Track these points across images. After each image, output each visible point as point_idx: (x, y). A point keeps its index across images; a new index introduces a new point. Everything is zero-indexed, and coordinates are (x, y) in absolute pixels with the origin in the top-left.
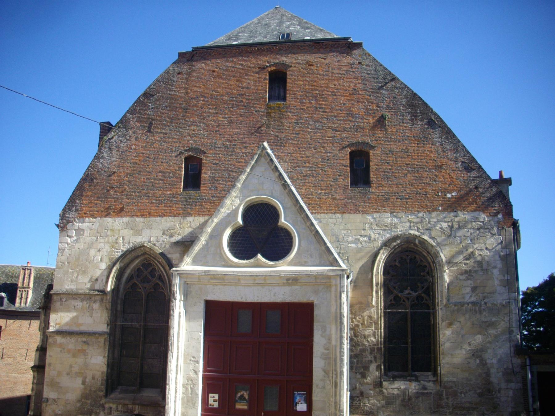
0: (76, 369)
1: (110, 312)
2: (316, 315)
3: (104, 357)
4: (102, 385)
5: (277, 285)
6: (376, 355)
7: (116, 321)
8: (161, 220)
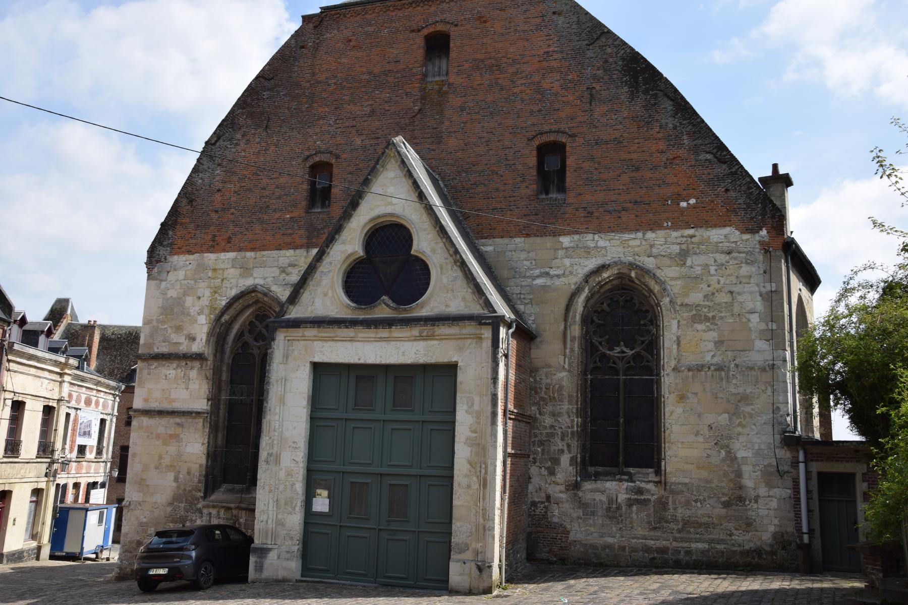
0: (167, 461)
3: (203, 444)
4: (199, 482)
5: (407, 339)
6: (570, 441)
8: (277, 254)
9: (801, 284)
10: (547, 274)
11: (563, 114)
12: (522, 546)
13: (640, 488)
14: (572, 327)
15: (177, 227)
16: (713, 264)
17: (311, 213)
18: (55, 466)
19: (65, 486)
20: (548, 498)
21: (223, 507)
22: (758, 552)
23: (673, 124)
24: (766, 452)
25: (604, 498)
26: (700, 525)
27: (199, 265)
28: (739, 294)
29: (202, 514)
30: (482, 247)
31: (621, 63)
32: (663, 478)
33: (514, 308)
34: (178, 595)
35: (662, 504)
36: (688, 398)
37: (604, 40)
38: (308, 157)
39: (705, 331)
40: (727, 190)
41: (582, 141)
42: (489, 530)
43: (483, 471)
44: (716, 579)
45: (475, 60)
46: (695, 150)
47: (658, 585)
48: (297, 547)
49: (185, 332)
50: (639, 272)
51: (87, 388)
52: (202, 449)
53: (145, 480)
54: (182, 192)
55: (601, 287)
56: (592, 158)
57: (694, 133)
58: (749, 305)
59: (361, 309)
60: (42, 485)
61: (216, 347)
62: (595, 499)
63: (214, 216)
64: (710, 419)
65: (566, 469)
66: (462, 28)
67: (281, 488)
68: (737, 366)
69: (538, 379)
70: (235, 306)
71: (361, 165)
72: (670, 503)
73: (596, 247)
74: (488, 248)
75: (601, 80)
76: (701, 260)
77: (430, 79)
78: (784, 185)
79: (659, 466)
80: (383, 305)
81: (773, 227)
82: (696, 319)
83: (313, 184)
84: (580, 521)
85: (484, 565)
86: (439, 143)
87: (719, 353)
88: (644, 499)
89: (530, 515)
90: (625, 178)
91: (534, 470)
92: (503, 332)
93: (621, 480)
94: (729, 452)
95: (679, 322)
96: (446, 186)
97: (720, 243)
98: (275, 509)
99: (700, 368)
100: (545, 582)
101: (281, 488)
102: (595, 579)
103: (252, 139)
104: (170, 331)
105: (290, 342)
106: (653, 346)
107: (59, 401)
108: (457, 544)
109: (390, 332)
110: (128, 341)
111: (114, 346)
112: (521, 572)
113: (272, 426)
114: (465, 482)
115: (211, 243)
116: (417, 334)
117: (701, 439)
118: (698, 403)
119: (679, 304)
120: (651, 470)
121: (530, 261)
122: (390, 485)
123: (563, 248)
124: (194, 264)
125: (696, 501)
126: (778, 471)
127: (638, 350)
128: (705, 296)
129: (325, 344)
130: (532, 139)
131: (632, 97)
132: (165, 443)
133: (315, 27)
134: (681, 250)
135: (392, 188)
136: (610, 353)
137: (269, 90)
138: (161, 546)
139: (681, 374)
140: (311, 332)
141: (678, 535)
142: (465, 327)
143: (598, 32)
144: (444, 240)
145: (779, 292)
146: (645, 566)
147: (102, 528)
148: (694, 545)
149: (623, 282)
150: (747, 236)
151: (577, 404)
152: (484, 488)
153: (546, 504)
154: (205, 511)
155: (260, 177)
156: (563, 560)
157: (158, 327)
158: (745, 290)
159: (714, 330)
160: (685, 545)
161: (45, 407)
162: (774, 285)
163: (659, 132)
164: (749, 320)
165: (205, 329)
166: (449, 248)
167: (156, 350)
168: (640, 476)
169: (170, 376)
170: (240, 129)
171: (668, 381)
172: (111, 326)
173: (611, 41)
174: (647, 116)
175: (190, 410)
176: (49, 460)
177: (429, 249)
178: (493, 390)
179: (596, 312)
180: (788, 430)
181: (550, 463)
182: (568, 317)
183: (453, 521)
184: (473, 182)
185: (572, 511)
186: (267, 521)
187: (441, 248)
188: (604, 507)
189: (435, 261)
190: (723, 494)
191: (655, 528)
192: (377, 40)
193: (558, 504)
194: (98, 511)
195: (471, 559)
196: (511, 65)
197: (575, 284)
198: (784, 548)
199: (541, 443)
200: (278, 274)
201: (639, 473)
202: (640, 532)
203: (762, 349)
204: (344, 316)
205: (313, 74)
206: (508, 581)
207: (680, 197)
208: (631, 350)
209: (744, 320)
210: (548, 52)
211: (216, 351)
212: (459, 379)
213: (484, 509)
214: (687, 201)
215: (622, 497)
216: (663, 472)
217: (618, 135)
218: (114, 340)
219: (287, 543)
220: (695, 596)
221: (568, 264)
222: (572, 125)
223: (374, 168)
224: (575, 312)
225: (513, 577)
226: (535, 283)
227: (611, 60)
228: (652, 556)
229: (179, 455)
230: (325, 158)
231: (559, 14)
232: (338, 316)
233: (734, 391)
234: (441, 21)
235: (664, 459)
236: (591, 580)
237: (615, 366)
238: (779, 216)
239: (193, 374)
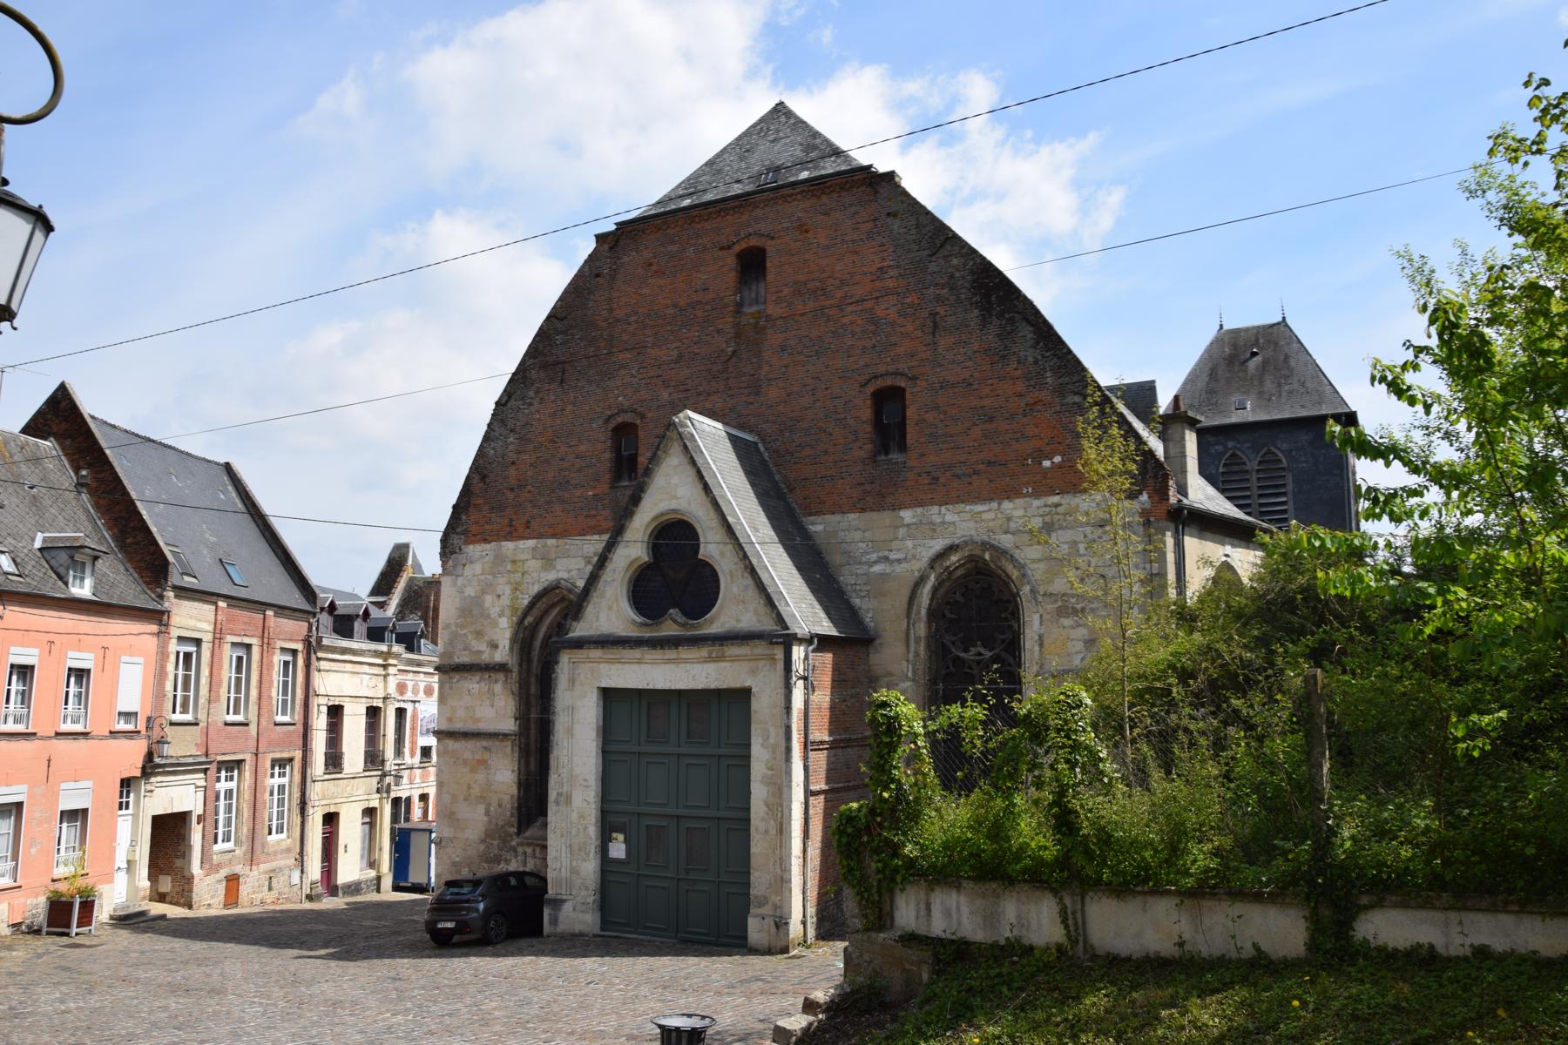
0: (476, 791)
1: (517, 698)
2: (755, 712)
3: (513, 771)
4: (512, 815)
7: (528, 712)
10: (886, 559)
11: (901, 350)
14: (917, 625)
16: (1083, 539)
18: (388, 780)
19: (408, 800)
21: (538, 845)
27: (496, 557)
38: (610, 417)
39: (1073, 628)
41: (924, 384)
45: (796, 282)
48: (592, 898)
51: (425, 673)
56: (936, 408)
57: (1060, 367)
60: (375, 804)
61: (521, 656)
63: (510, 495)
70: (538, 606)
73: (943, 523)
76: (1068, 535)
77: (747, 310)
81: (1155, 490)
82: (1063, 611)
86: (757, 394)
95: (1041, 616)
96: (767, 449)
101: (574, 832)
103: (546, 398)
104: (470, 637)
106: (1014, 646)
107: (385, 699)
108: (757, 897)
109: (678, 653)
123: (904, 525)
124: (491, 554)
129: (611, 666)
130: (866, 384)
131: (984, 323)
132: (473, 770)
133: (611, 248)
134: (1045, 523)
135: (676, 477)
136: (962, 655)
137: (562, 333)
140: (596, 653)
142: (755, 646)
143: (942, 238)
154: (520, 850)
161: (369, 709)
163: (1016, 369)
165: (508, 634)
167: (457, 660)
170: (532, 384)
173: (957, 248)
176: (379, 773)
179: (948, 603)
189: (725, 568)
196: (839, 288)
197: (919, 570)
200: (583, 565)
205: (611, 310)
207: (1042, 454)
208: (991, 651)
210: (881, 269)
211: (521, 660)
214: (1051, 459)
221: (911, 546)
222: (913, 364)
223: (655, 454)
224: (919, 606)
226: (872, 570)
227: (958, 274)
229: (489, 784)
232: (624, 634)
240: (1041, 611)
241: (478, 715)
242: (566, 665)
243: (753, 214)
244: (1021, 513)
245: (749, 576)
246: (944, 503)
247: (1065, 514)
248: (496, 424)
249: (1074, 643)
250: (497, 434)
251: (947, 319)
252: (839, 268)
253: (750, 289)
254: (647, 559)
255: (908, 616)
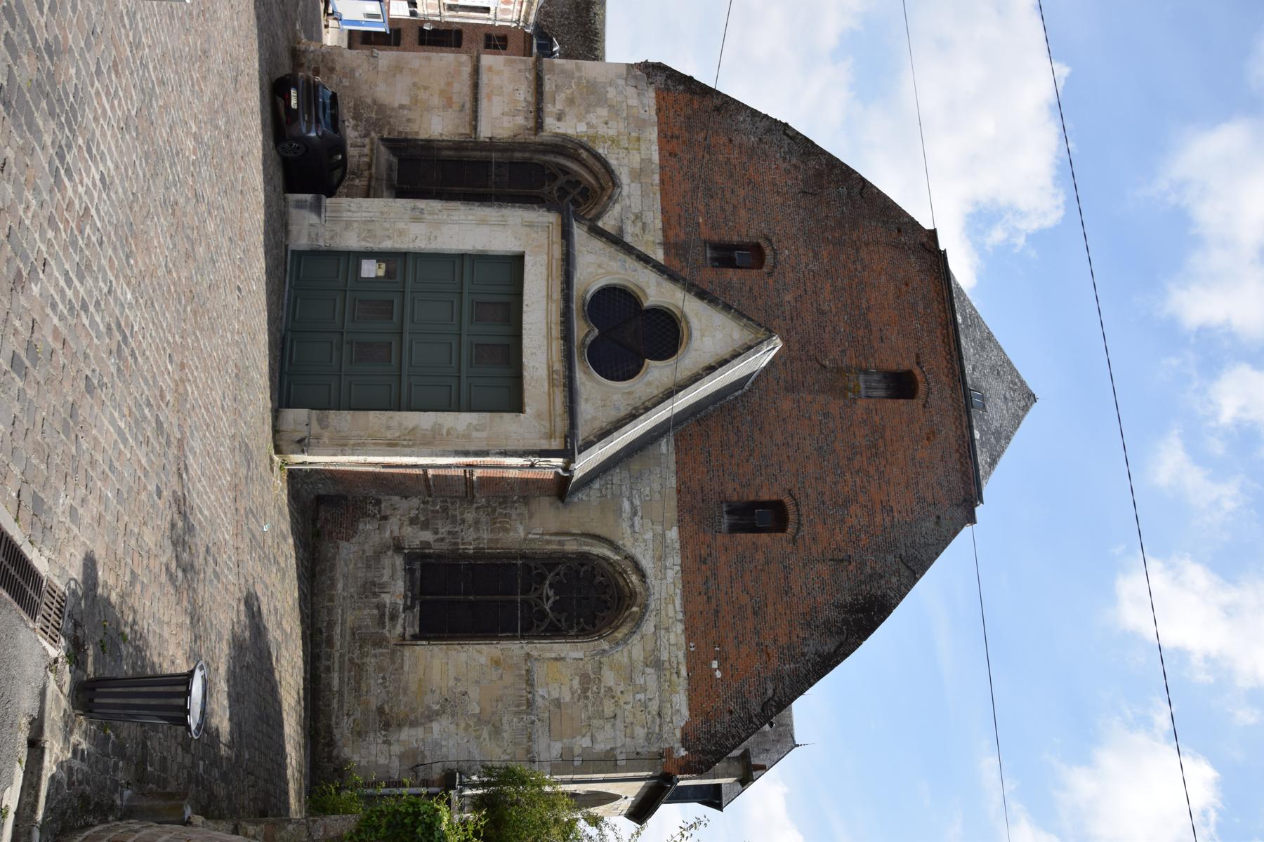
0: (423, 95)
1: (510, 140)
2: (501, 417)
3: (441, 135)
4: (400, 133)
9: (633, 799)
10: (635, 514)
12: (331, 490)
13: (397, 617)
14: (575, 542)
15: (688, 95)
16: (647, 697)
17: (705, 246)
20: (385, 518)
21: (371, 160)
22: (331, 743)
23: (807, 652)
24: (438, 753)
25: (385, 579)
26: (358, 682)
27: (644, 121)
28: (614, 725)
29: (364, 137)
30: (665, 440)
31: (879, 593)
32: (409, 642)
33: (596, 477)
34: (269, 121)
35: (380, 642)
36: (497, 670)
37: (906, 574)
38: (770, 241)
40: (731, 712)
41: (789, 550)
42: (342, 451)
43: (405, 443)
44: (298, 694)
46: (778, 677)
47: (289, 631)
49: (567, 109)
50: (637, 616)
52: (436, 134)
53: (401, 72)
54: (728, 99)
55: (620, 574)
56: (767, 562)
57: (798, 676)
58: (600, 737)
59: (584, 305)
61: (550, 145)
62: (384, 568)
64: (474, 693)
65: (417, 537)
66: (921, 412)
67: (387, 225)
68: (533, 722)
69: (517, 505)
70: (597, 163)
71: (760, 301)
72: (381, 650)
73: (666, 568)
74: (665, 447)
75: (859, 571)
76: (652, 683)
77: (862, 377)
78: (741, 777)
79: (421, 639)
80: (588, 330)
81: (689, 762)
82: (585, 679)
83: (739, 247)
84: (360, 553)
85: (305, 446)
86: (787, 390)
87: (547, 704)
88: (385, 622)
89: (366, 498)
90: (745, 599)
91: (415, 502)
92: (558, 461)
93: (405, 597)
94: (437, 713)
95: (581, 659)
96: (736, 398)
97: (671, 705)
98: (364, 219)
99: (530, 682)
100: (290, 511)
101: (387, 225)
102: (295, 566)
104: (568, 92)
105: (546, 229)
106: (555, 632)
109: (557, 339)
110: (587, 32)
111: (581, 17)
112: (302, 487)
113: (455, 213)
114: (394, 423)
115: (669, 134)
116: (555, 369)
117: (452, 683)
118: (491, 681)
119: (602, 659)
120: (417, 630)
121: (649, 494)
122: (391, 343)
124: (645, 116)
125: (383, 678)
126: (418, 766)
127: (550, 615)
128: (610, 689)
129: (544, 267)
130: (791, 495)
131: (839, 607)
132: (442, 92)
133: (923, 245)
137: (849, 193)
138: (321, 100)
139: (523, 662)
140: (557, 252)
141: (346, 658)
143: (915, 567)
144: (661, 396)
145: (616, 769)
146: (313, 624)
147: (361, 18)
148: (336, 675)
149: (627, 599)
150: (678, 734)
151: (488, 548)
152: (387, 444)
153: (378, 516)
154: (367, 141)
155: (746, 186)
156: (317, 534)
157: (573, 78)
158: (618, 732)
159: (573, 698)
160: (336, 666)
162: (624, 763)
163: (798, 637)
164: (584, 736)
165: (571, 132)
166: (651, 401)
167: (547, 77)
168: (411, 618)
169: (517, 95)
170: (803, 162)
171: (515, 649)
172: (605, 12)
174: (817, 623)
175: (479, 118)
177: (650, 379)
178: (493, 451)
179: (593, 568)
180: (463, 777)
181: (423, 519)
182: (586, 537)
183: (351, 412)
184: (740, 429)
185: (371, 544)
186: (349, 211)
187: (652, 392)
188: (376, 579)
189: (637, 386)
190: (392, 708)
191: (354, 634)
192: (907, 316)
193: (379, 528)
194: (380, 13)
195: (312, 432)
197: (623, 545)
198: (336, 770)
199: (445, 509)
201: (414, 617)
202: (350, 618)
203: (552, 751)
204: (575, 287)
205: (867, 244)
206: (291, 472)
208: (551, 608)
209: (584, 731)
211: (547, 145)
212: (505, 414)
213: (364, 445)
214: (718, 668)
215: (387, 599)
216: (414, 642)
217: (795, 591)
218: (588, 16)
219: (327, 233)
220: (274, 664)
222: (807, 540)
223: (744, 316)
224: (592, 545)
225: (296, 478)
226: (625, 500)
227: (883, 582)
228: (324, 630)
230: (769, 260)
231: (937, 523)
232: (575, 281)
233: (505, 720)
234: (930, 389)
235: (429, 644)
236: (294, 561)
237: (533, 589)
238: (702, 769)
239: (520, 120)
240: (586, 659)
241: (496, 99)
242: (545, 219)
243: (947, 387)
244: (673, 641)
245: (626, 412)
246: (684, 569)
247: (670, 681)
248: (768, 123)
249: (558, 689)
250: (758, 124)
251: (845, 571)
252: (895, 470)
253: (880, 381)
254: (645, 305)
255: (583, 535)
